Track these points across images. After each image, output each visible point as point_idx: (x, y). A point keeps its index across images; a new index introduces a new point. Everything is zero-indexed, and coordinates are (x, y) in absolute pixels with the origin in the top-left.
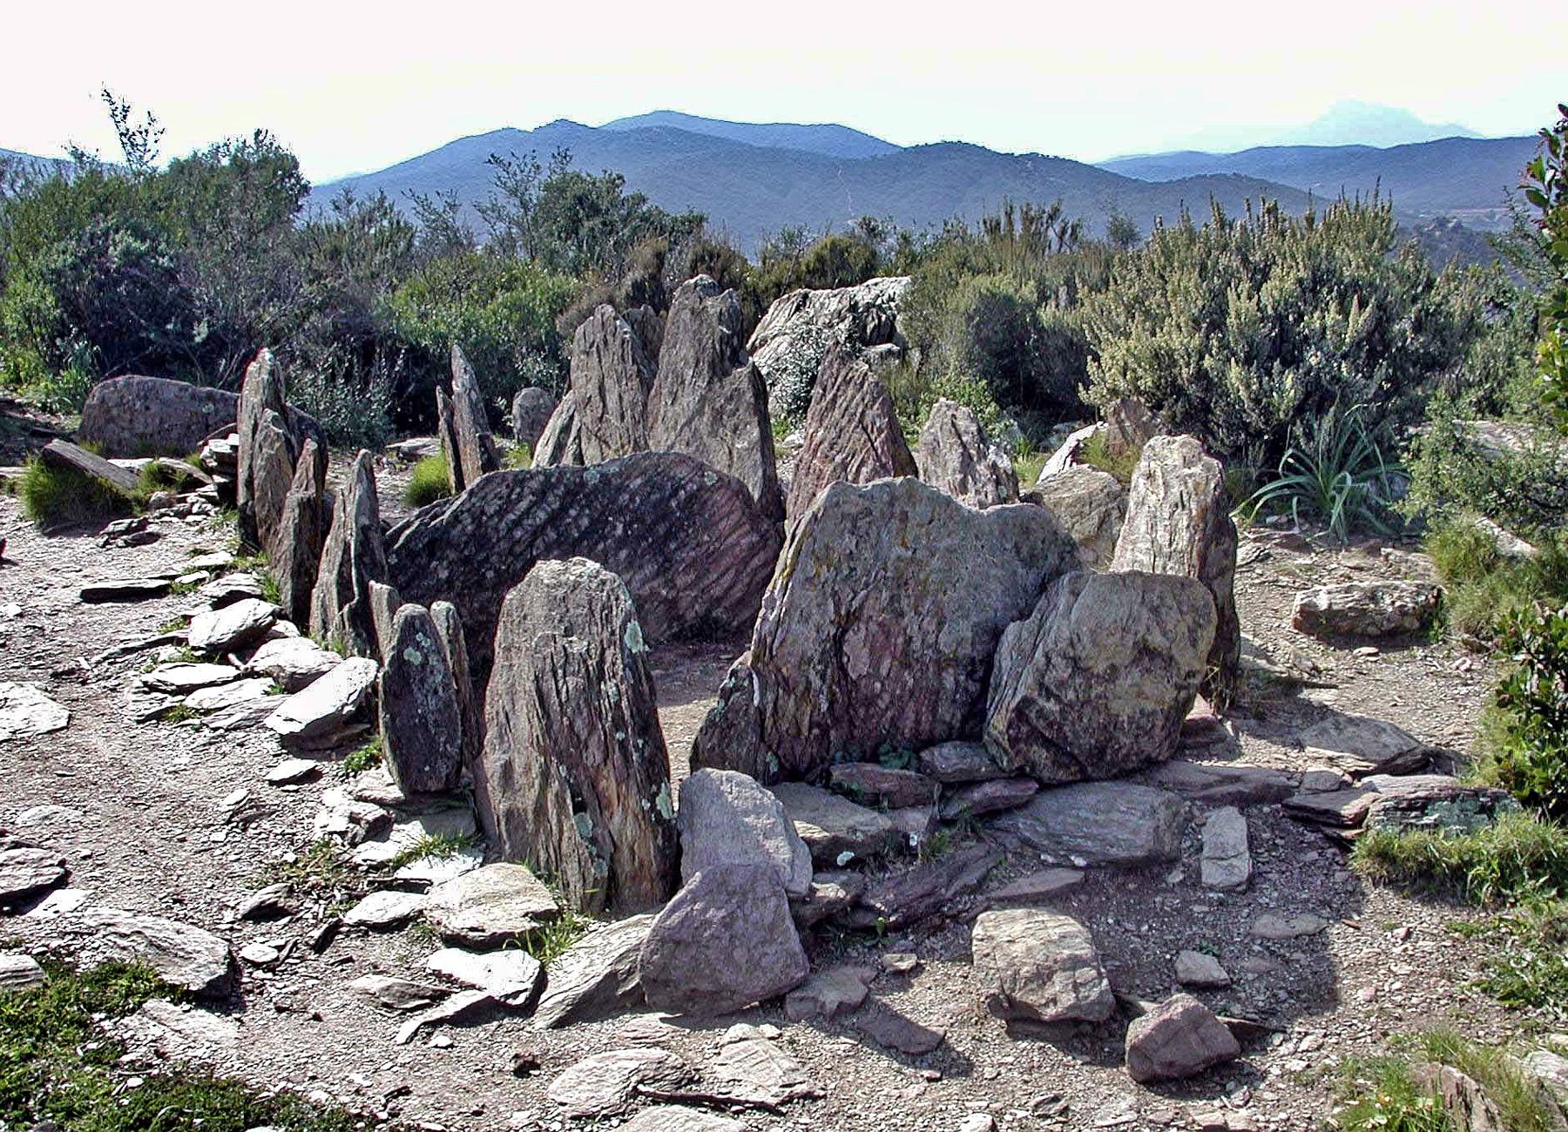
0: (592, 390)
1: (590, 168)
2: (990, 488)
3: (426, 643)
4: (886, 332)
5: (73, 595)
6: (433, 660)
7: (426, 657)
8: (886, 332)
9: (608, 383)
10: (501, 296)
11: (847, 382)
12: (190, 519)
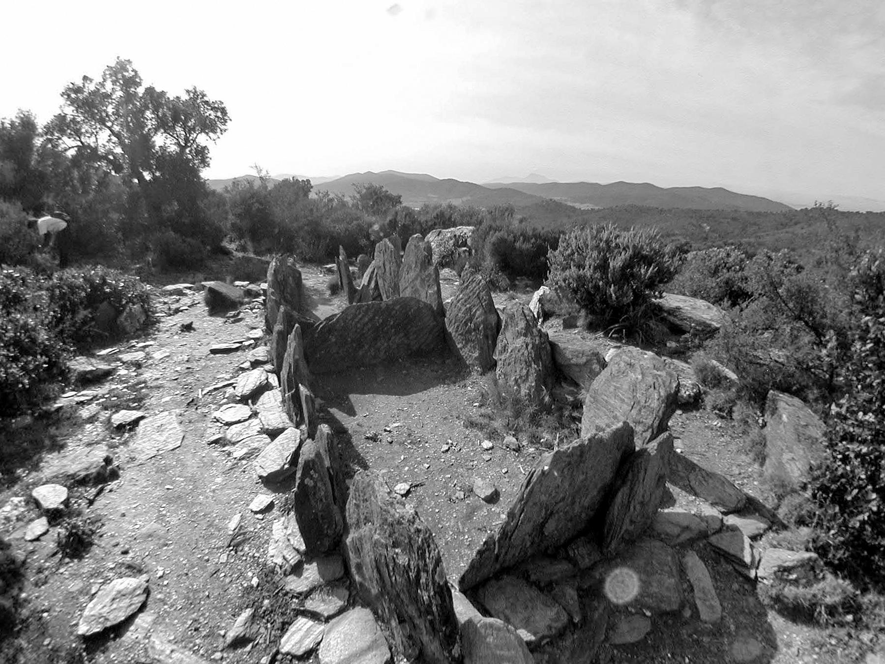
0: (381, 264)
1: (376, 184)
2: (537, 338)
3: (316, 476)
4: (465, 244)
5: (206, 350)
6: (319, 484)
7: (315, 483)
8: (465, 244)
9: (386, 263)
10: (355, 222)
11: (473, 281)
12: (254, 311)
